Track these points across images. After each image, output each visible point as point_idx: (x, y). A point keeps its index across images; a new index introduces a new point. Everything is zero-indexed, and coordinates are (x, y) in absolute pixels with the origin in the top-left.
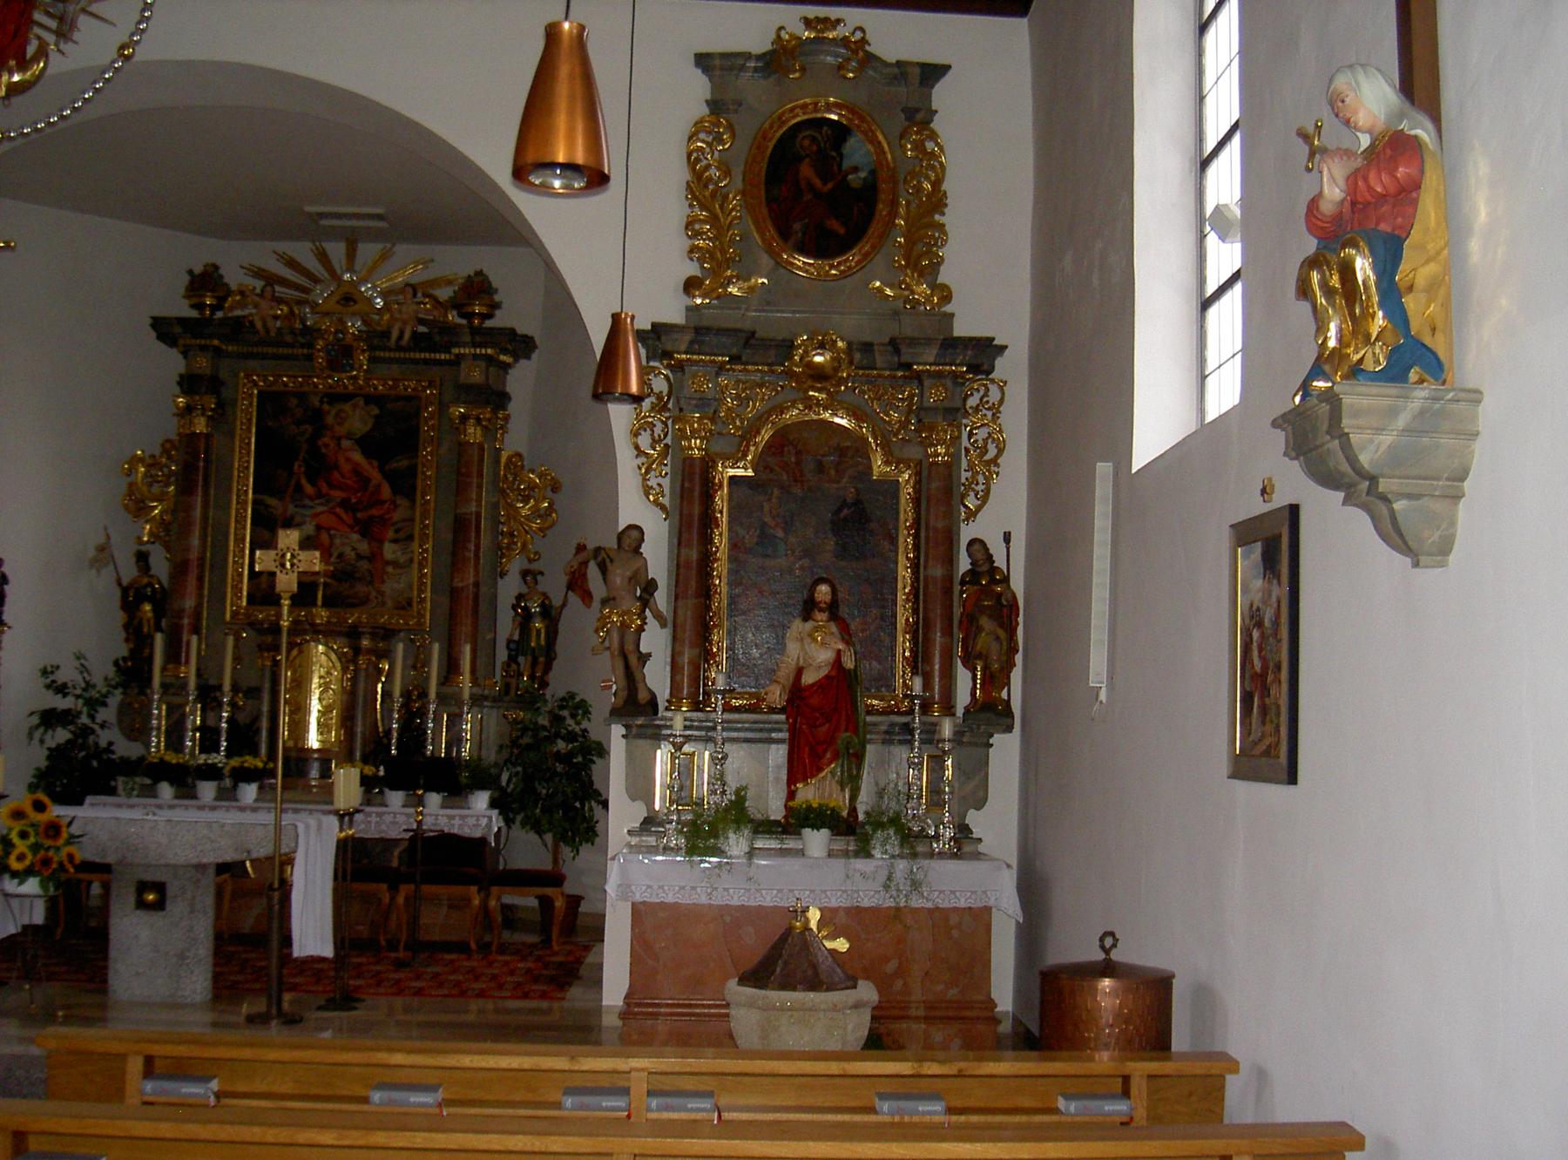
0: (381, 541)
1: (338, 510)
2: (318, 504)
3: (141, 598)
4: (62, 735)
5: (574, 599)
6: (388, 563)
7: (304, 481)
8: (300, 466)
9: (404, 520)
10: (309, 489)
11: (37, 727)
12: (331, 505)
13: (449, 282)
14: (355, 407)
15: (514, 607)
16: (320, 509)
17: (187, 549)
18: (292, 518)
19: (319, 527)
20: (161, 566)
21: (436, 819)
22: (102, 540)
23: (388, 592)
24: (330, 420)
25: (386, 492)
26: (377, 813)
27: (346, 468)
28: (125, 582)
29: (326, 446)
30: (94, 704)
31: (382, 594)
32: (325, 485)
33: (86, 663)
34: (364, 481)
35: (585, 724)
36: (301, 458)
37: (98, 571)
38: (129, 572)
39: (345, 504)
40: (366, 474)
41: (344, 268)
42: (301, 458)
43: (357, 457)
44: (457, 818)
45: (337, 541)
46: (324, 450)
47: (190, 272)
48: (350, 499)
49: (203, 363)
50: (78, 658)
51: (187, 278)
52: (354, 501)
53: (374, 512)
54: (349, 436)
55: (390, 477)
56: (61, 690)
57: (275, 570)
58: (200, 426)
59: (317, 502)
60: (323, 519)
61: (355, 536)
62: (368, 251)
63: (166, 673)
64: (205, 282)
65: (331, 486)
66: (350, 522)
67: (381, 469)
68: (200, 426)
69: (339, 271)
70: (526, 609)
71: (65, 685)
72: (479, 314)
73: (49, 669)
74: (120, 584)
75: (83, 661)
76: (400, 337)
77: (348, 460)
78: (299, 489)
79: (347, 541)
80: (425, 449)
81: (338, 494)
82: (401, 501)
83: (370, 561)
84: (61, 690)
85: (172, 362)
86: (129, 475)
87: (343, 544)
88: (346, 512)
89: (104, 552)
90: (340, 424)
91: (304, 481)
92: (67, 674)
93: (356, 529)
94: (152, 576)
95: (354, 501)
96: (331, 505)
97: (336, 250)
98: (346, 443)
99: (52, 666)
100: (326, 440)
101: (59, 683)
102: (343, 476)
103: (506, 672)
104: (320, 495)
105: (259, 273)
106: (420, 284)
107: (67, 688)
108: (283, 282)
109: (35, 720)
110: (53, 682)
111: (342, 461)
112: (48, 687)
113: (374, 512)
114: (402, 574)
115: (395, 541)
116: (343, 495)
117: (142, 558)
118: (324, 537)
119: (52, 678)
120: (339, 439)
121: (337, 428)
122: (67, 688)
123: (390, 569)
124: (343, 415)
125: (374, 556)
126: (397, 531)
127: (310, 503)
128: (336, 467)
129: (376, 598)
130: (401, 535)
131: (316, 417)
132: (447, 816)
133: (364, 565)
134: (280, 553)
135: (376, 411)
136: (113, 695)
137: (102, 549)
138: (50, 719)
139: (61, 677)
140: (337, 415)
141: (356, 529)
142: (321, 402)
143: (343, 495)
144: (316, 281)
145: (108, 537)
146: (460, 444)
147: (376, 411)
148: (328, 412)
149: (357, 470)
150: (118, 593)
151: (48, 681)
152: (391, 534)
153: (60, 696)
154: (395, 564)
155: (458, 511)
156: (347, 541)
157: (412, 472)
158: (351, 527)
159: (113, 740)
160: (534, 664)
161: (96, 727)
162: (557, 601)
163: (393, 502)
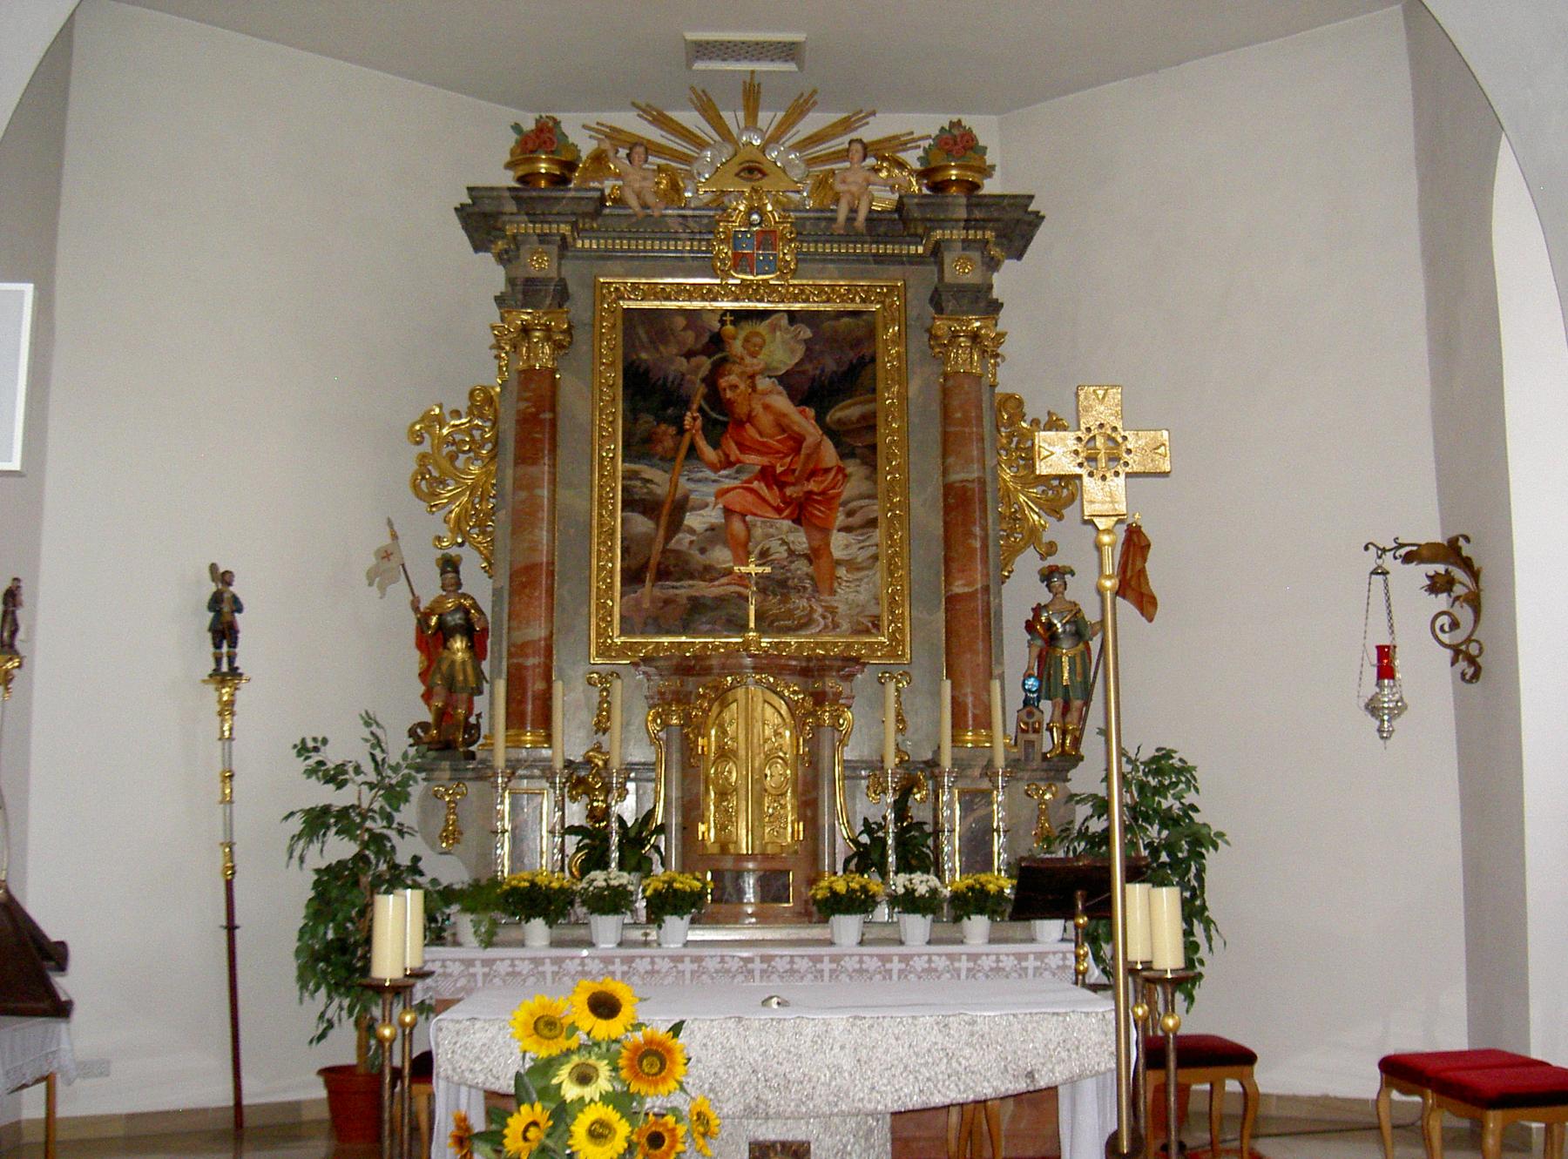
0: (826, 531)
1: (755, 484)
2: (727, 477)
3: (444, 633)
4: (340, 848)
5: (1126, 608)
6: (839, 563)
7: (702, 444)
8: (695, 419)
9: (861, 497)
10: (709, 453)
11: (300, 836)
12: (745, 477)
13: (929, 137)
14: (774, 328)
15: (1030, 626)
16: (728, 483)
17: (534, 548)
18: (686, 498)
19: (728, 512)
20: (478, 585)
21: (998, 961)
22: (385, 540)
23: (842, 608)
24: (737, 347)
25: (829, 455)
26: (900, 955)
27: (766, 421)
28: (424, 605)
29: (734, 387)
30: (396, 795)
31: (832, 610)
32: (733, 445)
33: (379, 732)
34: (797, 440)
35: (1190, 798)
36: (695, 407)
37: (382, 589)
38: (430, 589)
39: (766, 474)
40: (796, 428)
41: (742, 125)
42: (695, 407)
43: (782, 402)
44: (1031, 957)
45: (758, 532)
46: (729, 394)
47: (517, 128)
48: (773, 467)
49: (540, 264)
50: (368, 724)
51: (512, 138)
52: (779, 470)
53: (812, 486)
54: (767, 371)
55: (834, 433)
56: (336, 777)
57: (1078, 471)
58: (544, 355)
59: (723, 472)
60: (739, 500)
61: (787, 524)
62: (768, 118)
63: (728, 318)
64: (543, 137)
65: (743, 448)
66: (777, 502)
67: (819, 419)
68: (544, 355)
69: (735, 131)
70: (1050, 626)
71: (341, 769)
72: (958, 182)
73: (310, 744)
74: (416, 609)
75: (374, 728)
76: (850, 220)
77: (767, 407)
78: (693, 451)
79: (771, 531)
80: (888, 389)
81: (755, 461)
82: (852, 467)
83: (811, 562)
84: (336, 777)
85: (490, 274)
86: (418, 443)
87: (768, 536)
88: (769, 487)
89: (388, 563)
90: (754, 355)
91: (702, 444)
92: (346, 747)
93: (786, 513)
94: (465, 596)
95: (779, 470)
96: (745, 477)
97: (733, 118)
98: (763, 383)
99: (315, 739)
100: (733, 379)
101: (331, 765)
102: (761, 434)
103: (1026, 724)
104: (728, 464)
105: (615, 135)
106: (873, 143)
107: (346, 772)
108: (660, 150)
109: (297, 824)
110: (321, 763)
111: (758, 409)
112: (310, 772)
113: (812, 486)
114: (860, 580)
115: (847, 529)
116: (764, 461)
117: (449, 565)
118: (737, 526)
119: (316, 758)
120: (752, 377)
121: (748, 360)
122: (346, 772)
123: (842, 572)
124: (757, 340)
125: (815, 555)
126: (850, 514)
127: (713, 476)
128: (750, 418)
129: (824, 617)
130: (856, 520)
131: (717, 342)
132: (462, 961)
133: (802, 567)
134: (1085, 437)
135: (807, 333)
136: (416, 781)
137: (386, 555)
138: (317, 821)
139: (332, 756)
140: (747, 340)
141: (786, 513)
142: (723, 323)
143: (764, 461)
144: (701, 145)
145: (395, 536)
146: (946, 376)
147: (807, 333)
148: (734, 338)
149: (782, 425)
150: (412, 621)
151: (311, 762)
152: (840, 519)
153: (331, 786)
154: (851, 565)
155: (954, 477)
156: (771, 531)
157: (868, 424)
158: (779, 510)
159: (419, 854)
160: (1066, 709)
161: (392, 834)
162: (1091, 615)
163: (840, 470)
